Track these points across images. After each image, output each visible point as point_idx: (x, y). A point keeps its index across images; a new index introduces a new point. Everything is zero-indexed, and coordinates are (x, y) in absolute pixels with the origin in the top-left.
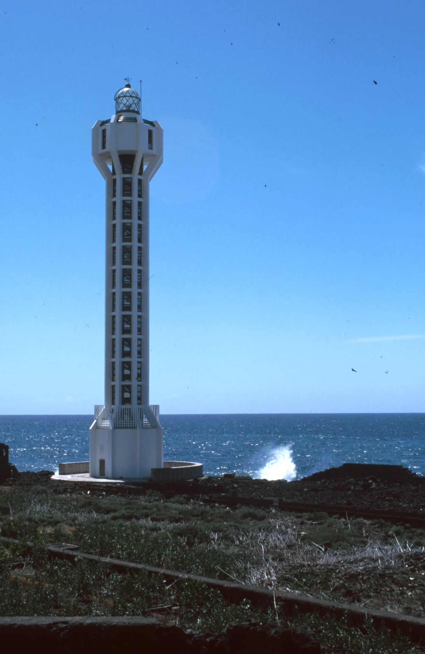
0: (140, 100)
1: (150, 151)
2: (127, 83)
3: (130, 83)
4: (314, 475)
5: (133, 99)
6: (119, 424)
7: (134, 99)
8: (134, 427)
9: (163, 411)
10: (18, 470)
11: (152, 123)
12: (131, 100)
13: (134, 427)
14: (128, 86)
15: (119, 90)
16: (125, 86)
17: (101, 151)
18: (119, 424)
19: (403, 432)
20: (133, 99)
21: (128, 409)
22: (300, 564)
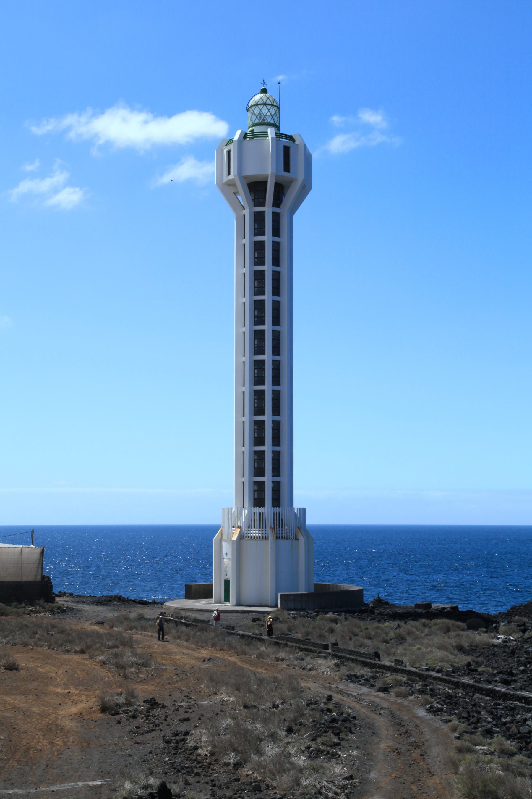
0: (278, 108)
1: (286, 174)
2: (263, 88)
3: (266, 87)
4: (450, 620)
5: (259, 107)
6: (279, 534)
7: (269, 107)
8: (266, 537)
9: (311, 520)
10: (479, 612)
11: (290, 138)
12: (265, 110)
13: (266, 537)
14: (264, 91)
15: (251, 99)
16: (260, 91)
17: (226, 178)
18: (279, 534)
19: (401, 554)
20: (259, 107)
21: (276, 513)
22: (57, 688)
